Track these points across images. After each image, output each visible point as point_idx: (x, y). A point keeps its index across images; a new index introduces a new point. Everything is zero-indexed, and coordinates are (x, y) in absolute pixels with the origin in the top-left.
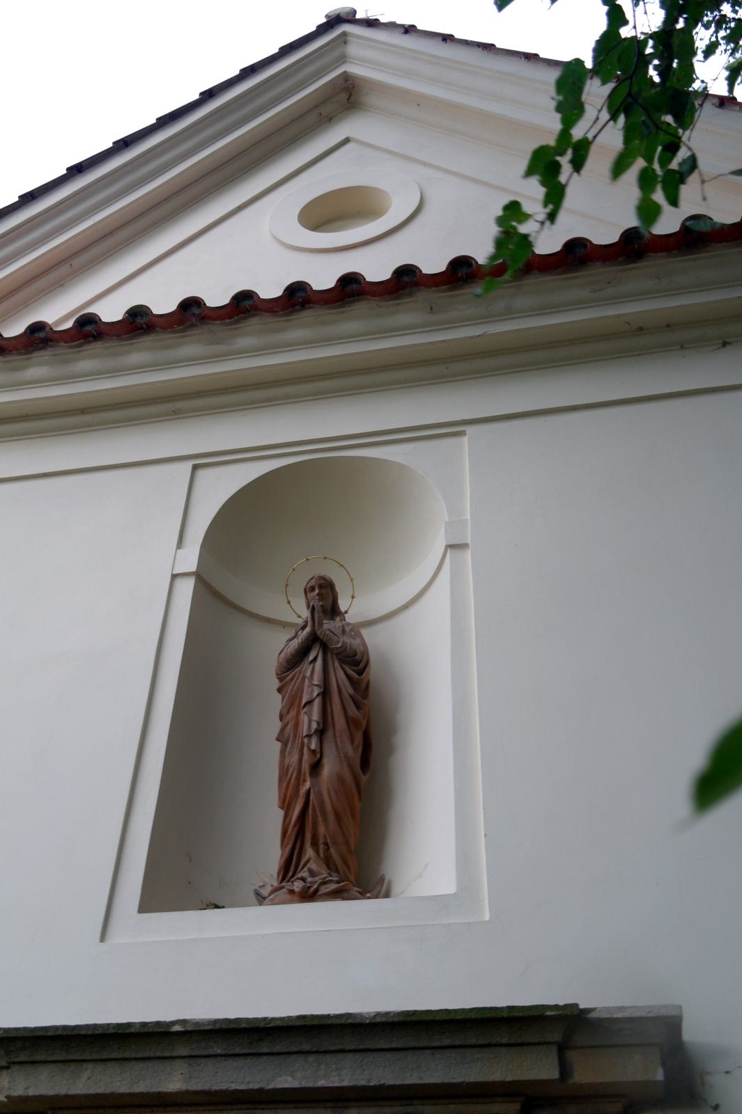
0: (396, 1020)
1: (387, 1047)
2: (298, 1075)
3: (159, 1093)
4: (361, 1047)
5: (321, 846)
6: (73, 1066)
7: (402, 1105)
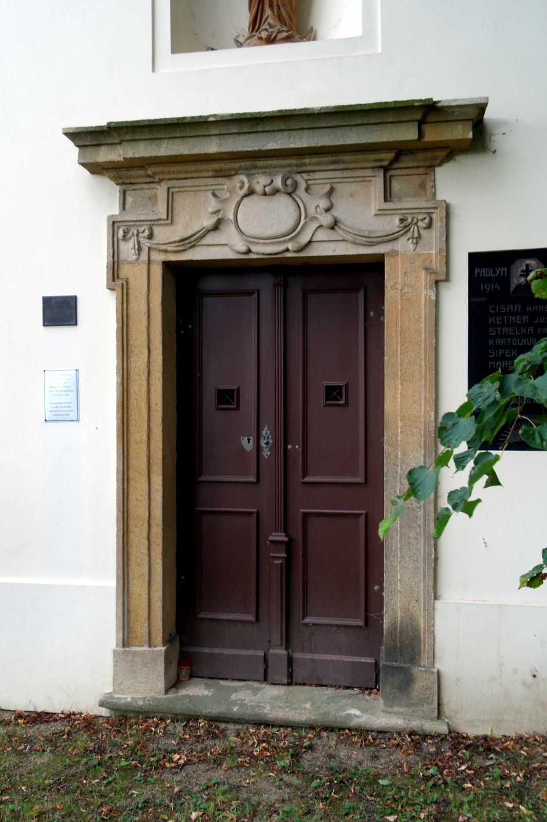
0: (332, 111)
1: (327, 126)
2: (279, 142)
3: (206, 154)
4: (313, 126)
5: (275, 8)
6: (156, 142)
7: (333, 156)
